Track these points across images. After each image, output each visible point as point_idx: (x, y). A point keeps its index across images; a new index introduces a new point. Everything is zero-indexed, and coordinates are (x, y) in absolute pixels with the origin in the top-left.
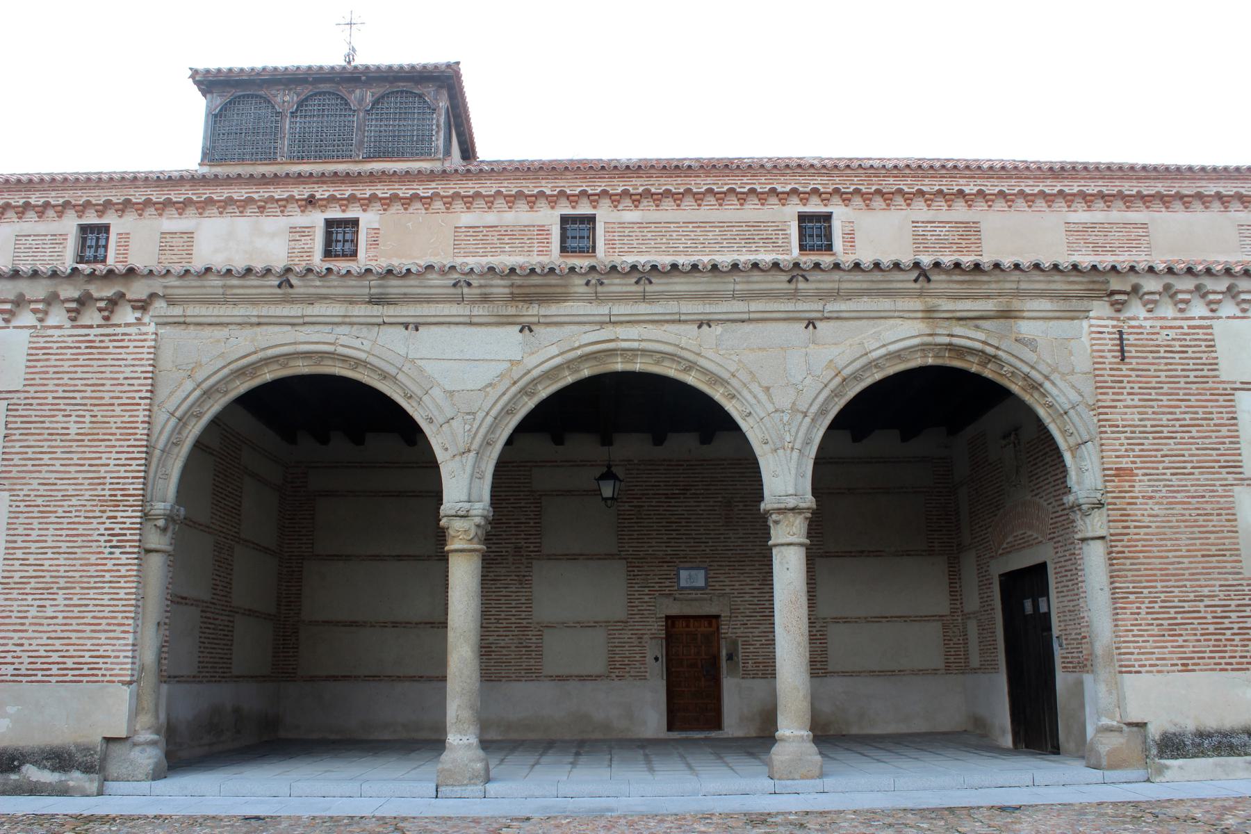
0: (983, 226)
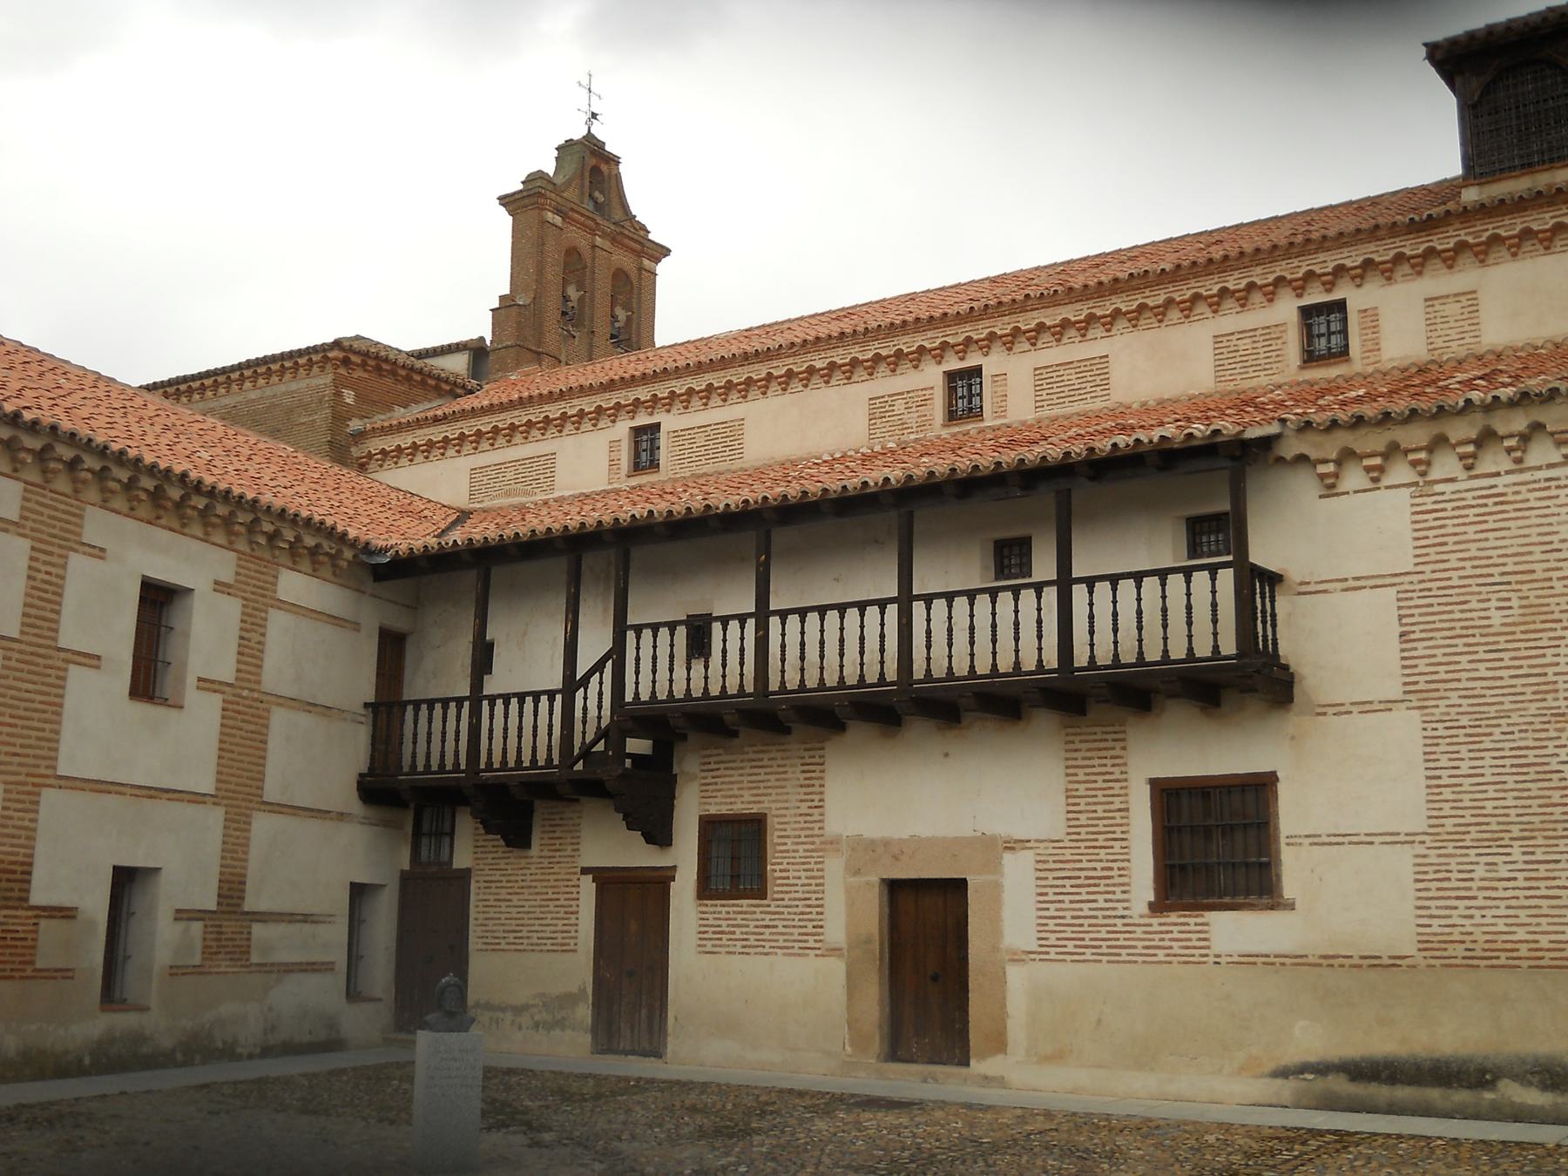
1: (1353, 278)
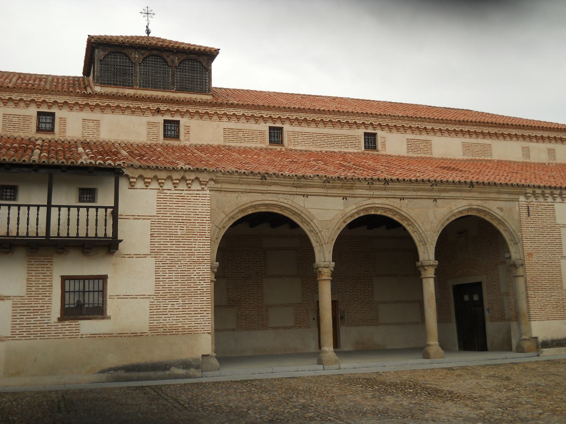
0: (433, 142)
1: (59, 106)
